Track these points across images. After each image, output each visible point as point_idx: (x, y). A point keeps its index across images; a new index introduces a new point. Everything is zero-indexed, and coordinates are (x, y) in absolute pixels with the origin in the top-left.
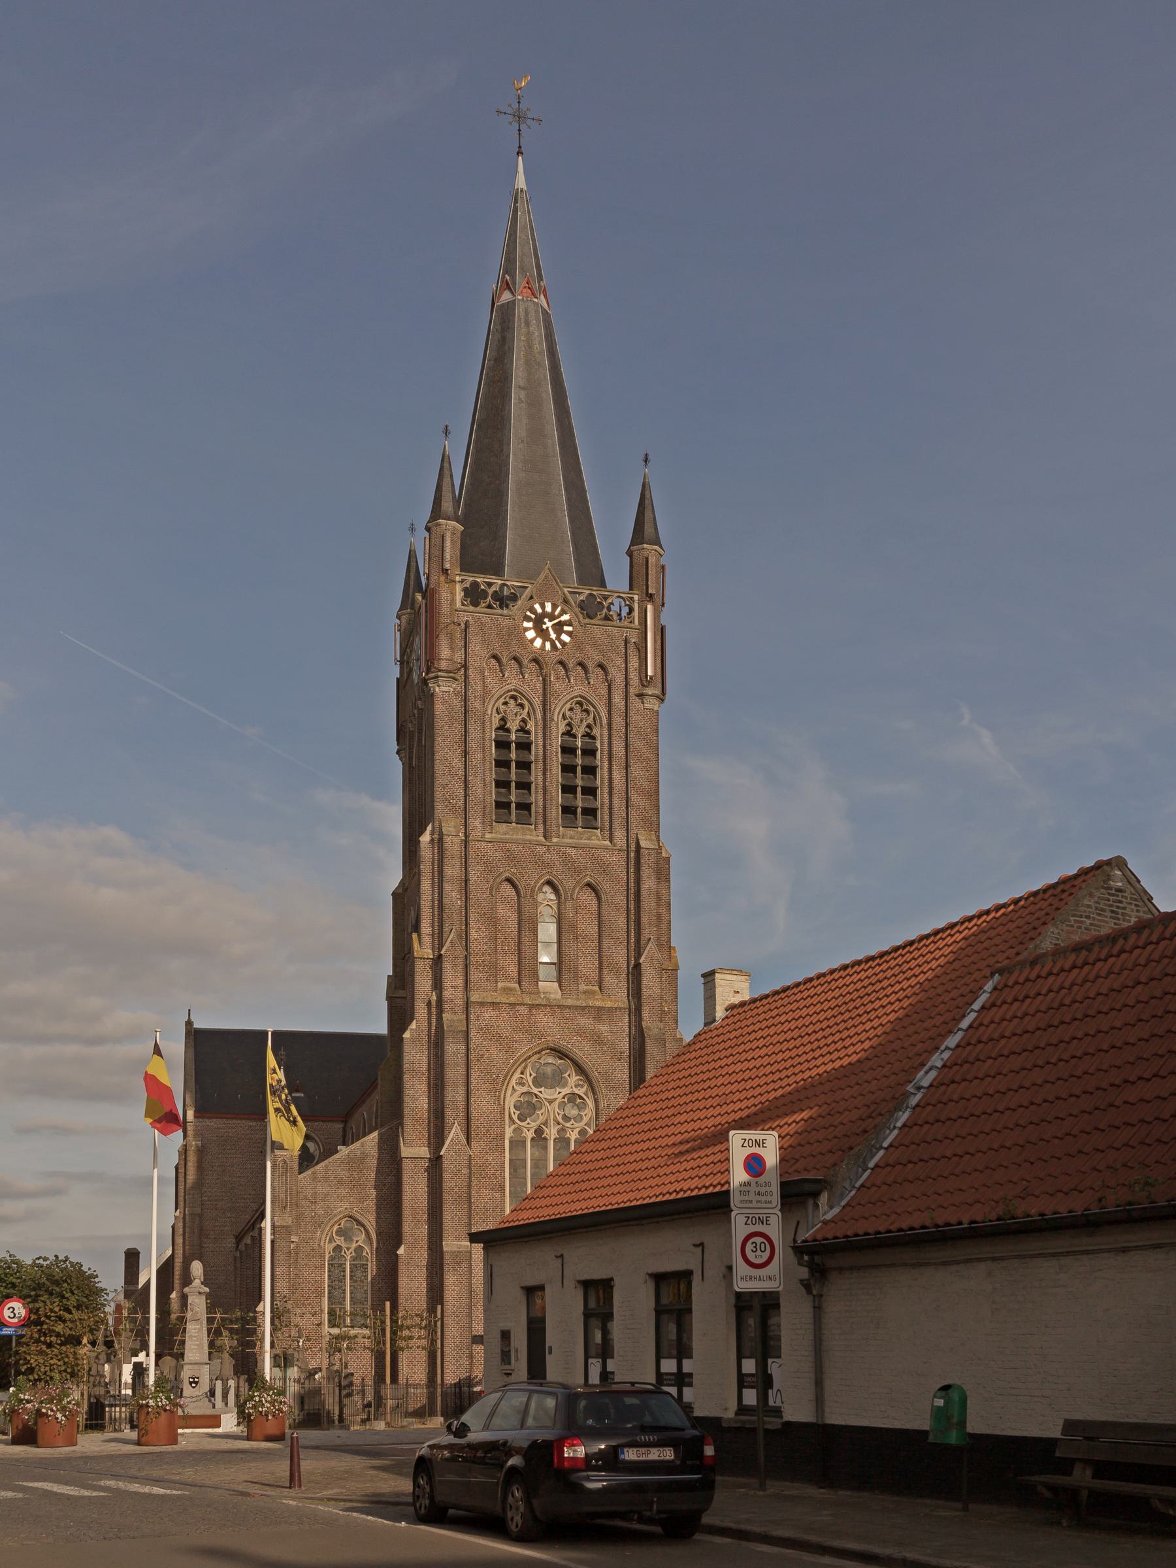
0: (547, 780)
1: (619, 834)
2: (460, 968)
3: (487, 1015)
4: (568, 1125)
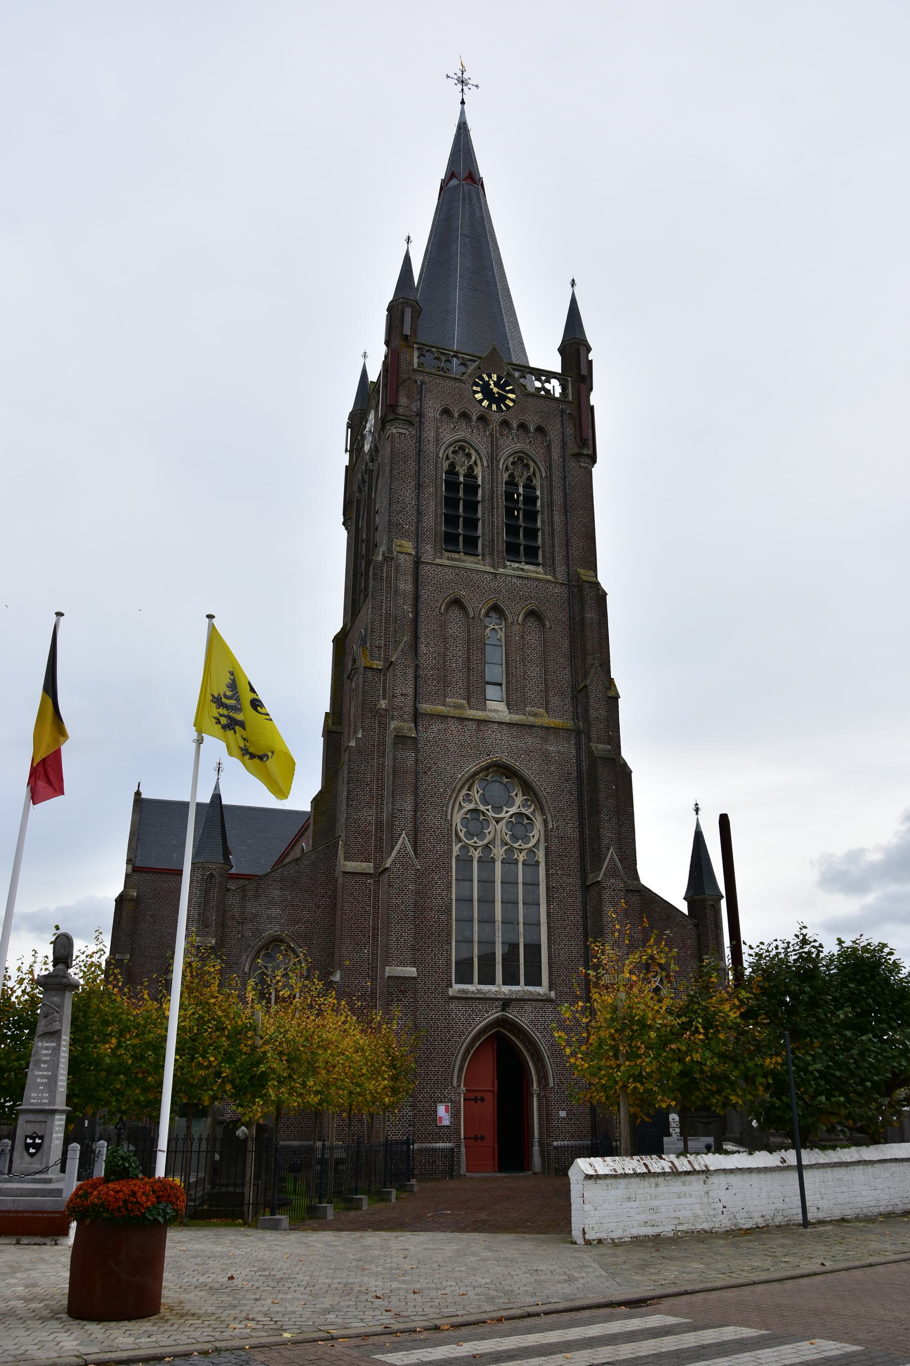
0: (491, 521)
1: (561, 570)
2: (410, 677)
3: (435, 728)
4: (516, 845)
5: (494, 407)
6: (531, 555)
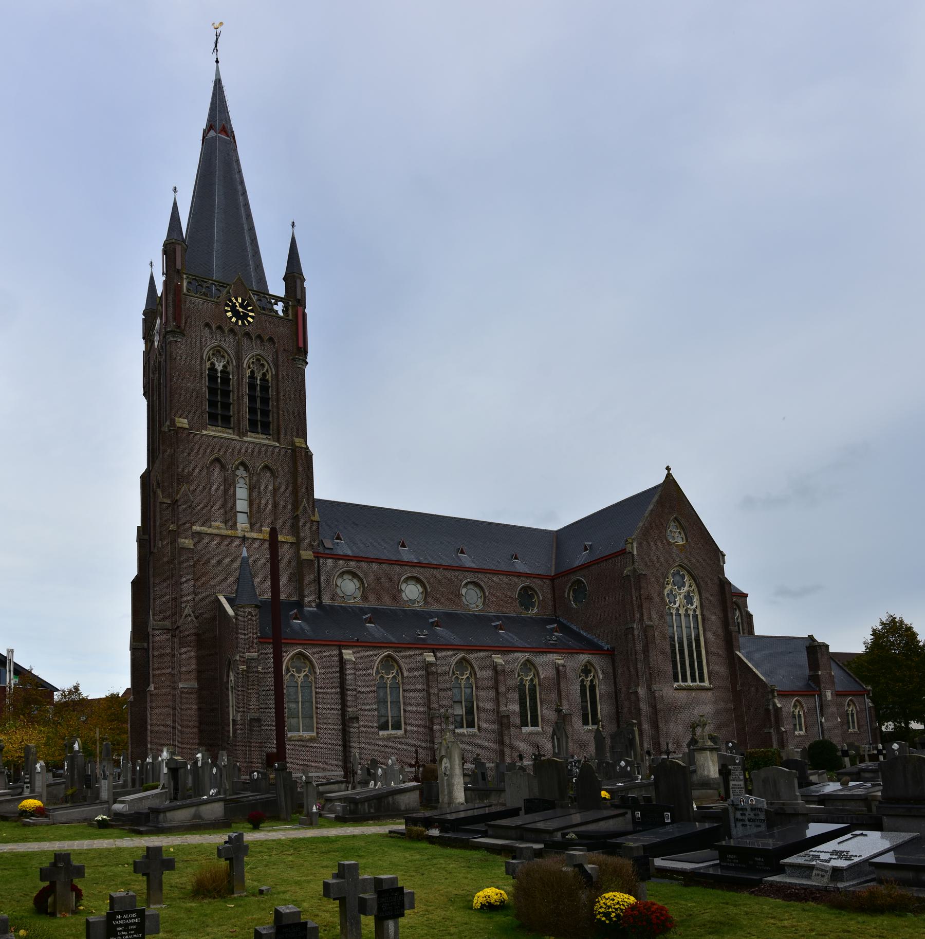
5: (240, 322)
6: (265, 428)
